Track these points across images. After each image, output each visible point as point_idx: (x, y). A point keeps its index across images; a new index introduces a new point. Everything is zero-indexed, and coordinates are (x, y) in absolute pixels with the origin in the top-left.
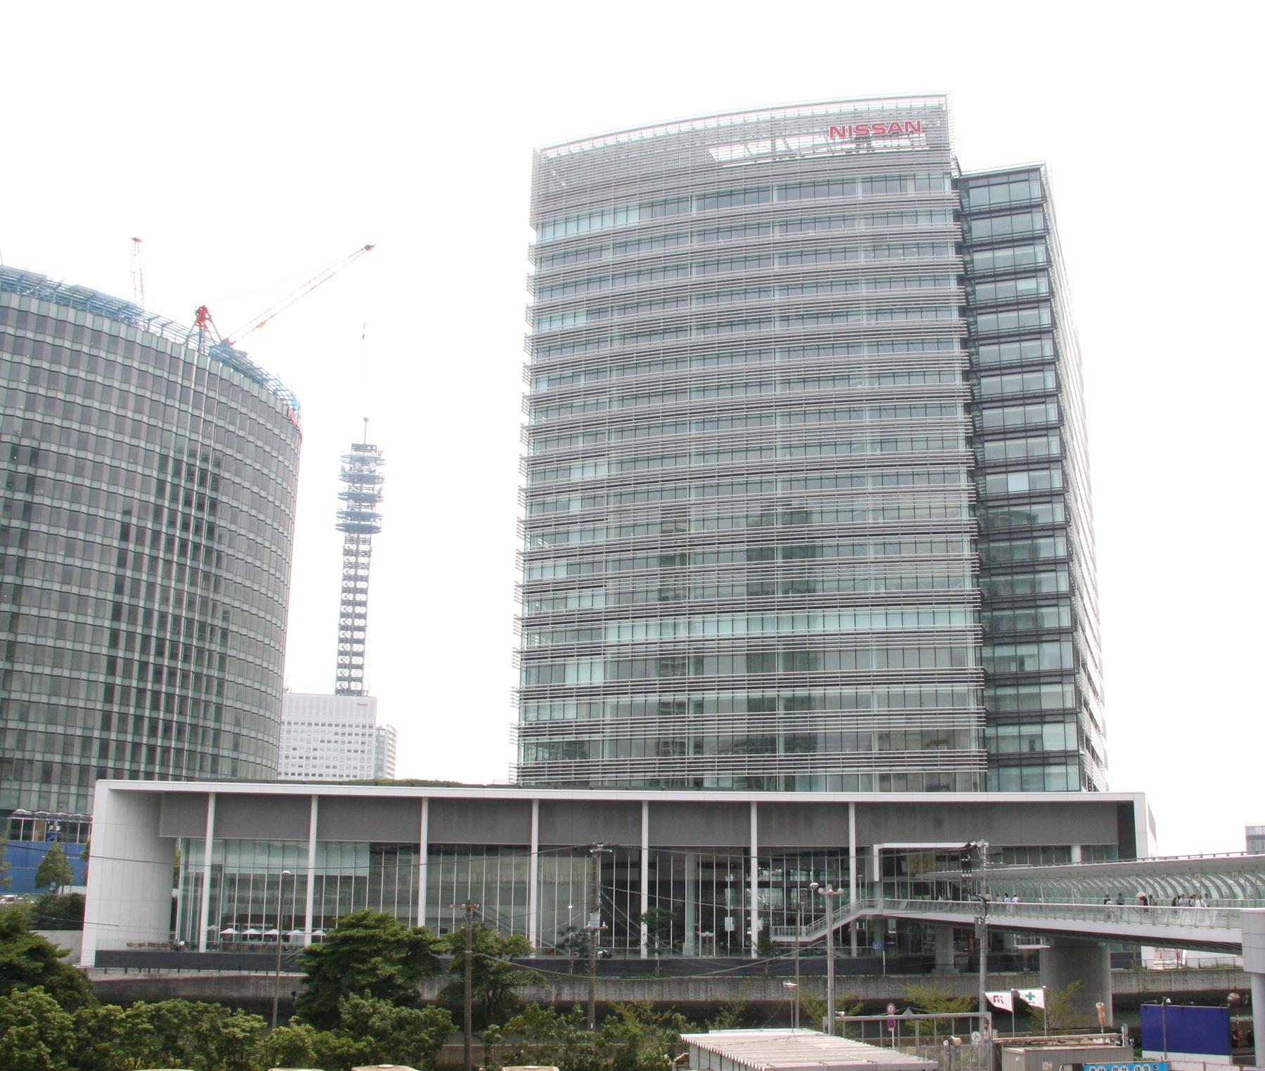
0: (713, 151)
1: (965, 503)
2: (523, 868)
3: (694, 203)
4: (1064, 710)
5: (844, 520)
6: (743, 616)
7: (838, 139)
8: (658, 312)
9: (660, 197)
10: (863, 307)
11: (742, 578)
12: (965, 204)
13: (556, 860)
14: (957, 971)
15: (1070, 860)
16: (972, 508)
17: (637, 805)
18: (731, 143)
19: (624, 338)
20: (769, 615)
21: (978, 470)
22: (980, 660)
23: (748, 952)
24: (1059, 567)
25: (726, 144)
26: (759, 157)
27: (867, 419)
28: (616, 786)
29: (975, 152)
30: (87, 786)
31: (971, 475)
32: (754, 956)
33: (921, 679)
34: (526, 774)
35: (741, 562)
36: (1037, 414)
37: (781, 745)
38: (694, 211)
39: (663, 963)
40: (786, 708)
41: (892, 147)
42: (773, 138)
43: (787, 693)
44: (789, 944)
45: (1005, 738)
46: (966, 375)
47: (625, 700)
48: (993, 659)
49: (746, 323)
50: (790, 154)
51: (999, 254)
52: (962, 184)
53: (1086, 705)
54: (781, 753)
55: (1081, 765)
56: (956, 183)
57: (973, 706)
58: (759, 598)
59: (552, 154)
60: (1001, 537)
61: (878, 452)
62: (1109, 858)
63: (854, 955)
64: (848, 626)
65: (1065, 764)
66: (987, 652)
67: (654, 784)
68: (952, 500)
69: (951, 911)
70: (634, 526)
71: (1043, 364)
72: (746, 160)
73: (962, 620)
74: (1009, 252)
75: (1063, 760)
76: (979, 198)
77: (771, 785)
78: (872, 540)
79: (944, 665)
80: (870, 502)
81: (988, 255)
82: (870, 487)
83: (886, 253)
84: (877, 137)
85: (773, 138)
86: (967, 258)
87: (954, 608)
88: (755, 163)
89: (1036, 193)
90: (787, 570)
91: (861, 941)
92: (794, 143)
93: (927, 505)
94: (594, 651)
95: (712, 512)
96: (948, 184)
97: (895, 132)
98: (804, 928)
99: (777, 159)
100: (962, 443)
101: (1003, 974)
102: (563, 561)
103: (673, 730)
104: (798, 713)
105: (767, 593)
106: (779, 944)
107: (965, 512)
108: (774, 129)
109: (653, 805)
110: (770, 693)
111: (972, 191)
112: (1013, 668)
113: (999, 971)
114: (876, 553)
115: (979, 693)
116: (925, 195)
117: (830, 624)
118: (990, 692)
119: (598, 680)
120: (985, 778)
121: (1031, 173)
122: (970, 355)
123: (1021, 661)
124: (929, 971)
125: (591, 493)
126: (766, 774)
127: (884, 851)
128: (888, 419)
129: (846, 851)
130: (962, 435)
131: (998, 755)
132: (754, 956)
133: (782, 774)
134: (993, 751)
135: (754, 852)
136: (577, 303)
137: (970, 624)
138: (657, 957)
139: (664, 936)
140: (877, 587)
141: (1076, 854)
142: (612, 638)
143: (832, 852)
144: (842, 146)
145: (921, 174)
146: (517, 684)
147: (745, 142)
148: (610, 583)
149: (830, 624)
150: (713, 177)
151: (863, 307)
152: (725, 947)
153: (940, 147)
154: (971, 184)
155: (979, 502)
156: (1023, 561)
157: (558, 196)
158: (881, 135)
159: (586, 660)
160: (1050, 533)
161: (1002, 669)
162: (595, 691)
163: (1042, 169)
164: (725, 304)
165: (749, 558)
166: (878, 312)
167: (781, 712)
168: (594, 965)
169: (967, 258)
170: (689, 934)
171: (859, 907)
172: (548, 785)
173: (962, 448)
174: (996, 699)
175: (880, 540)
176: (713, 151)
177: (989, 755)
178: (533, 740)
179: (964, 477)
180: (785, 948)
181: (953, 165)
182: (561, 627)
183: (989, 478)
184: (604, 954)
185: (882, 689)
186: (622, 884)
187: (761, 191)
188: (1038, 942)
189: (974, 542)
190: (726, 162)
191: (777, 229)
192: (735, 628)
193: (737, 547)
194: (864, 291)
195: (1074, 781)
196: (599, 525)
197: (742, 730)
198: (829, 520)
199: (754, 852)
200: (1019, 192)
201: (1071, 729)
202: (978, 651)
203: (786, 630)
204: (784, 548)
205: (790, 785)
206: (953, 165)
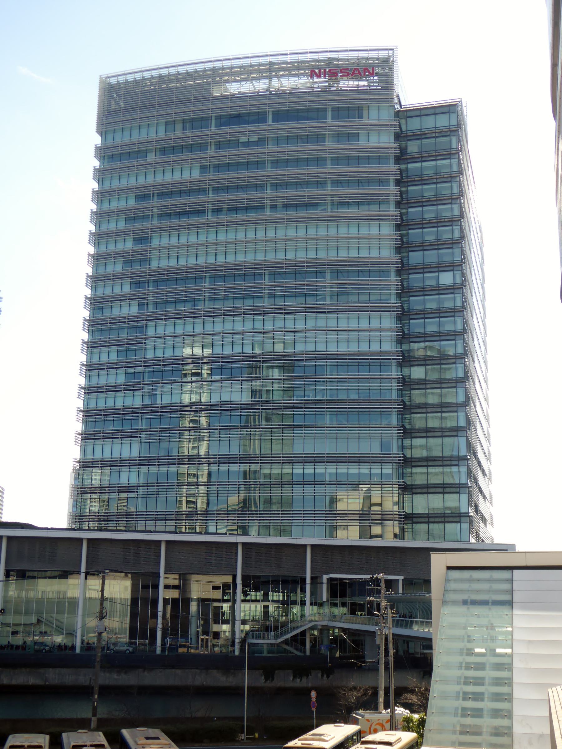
8: (186, 200)
10: (329, 200)
12: (404, 128)
29: (414, 89)
34: (78, 518)
36: (448, 325)
38: (213, 128)
46: (398, 204)
53: (476, 481)
55: (470, 494)
56: (397, 114)
59: (113, 81)
63: (308, 653)
76: (414, 125)
78: (329, 363)
79: (376, 449)
85: (270, 78)
86: (404, 189)
87: (384, 315)
88: (258, 96)
89: (457, 235)
98: (273, 633)
99: (271, 95)
102: (115, 349)
108: (271, 70)
115: (400, 471)
119: (135, 453)
121: (451, 109)
122: (402, 236)
125: (134, 324)
127: (330, 580)
128: (342, 280)
136: (128, 190)
137: (394, 325)
140: (331, 420)
146: (78, 457)
148: (146, 388)
151: (329, 200)
153: (387, 84)
156: (431, 286)
162: (136, 411)
169: (404, 189)
173: (393, 300)
175: (334, 363)
181: (396, 101)
182: (110, 418)
186: (145, 600)
187: (261, 118)
194: (329, 168)
196: (139, 347)
200: (442, 121)
202: (400, 441)
206: (396, 101)
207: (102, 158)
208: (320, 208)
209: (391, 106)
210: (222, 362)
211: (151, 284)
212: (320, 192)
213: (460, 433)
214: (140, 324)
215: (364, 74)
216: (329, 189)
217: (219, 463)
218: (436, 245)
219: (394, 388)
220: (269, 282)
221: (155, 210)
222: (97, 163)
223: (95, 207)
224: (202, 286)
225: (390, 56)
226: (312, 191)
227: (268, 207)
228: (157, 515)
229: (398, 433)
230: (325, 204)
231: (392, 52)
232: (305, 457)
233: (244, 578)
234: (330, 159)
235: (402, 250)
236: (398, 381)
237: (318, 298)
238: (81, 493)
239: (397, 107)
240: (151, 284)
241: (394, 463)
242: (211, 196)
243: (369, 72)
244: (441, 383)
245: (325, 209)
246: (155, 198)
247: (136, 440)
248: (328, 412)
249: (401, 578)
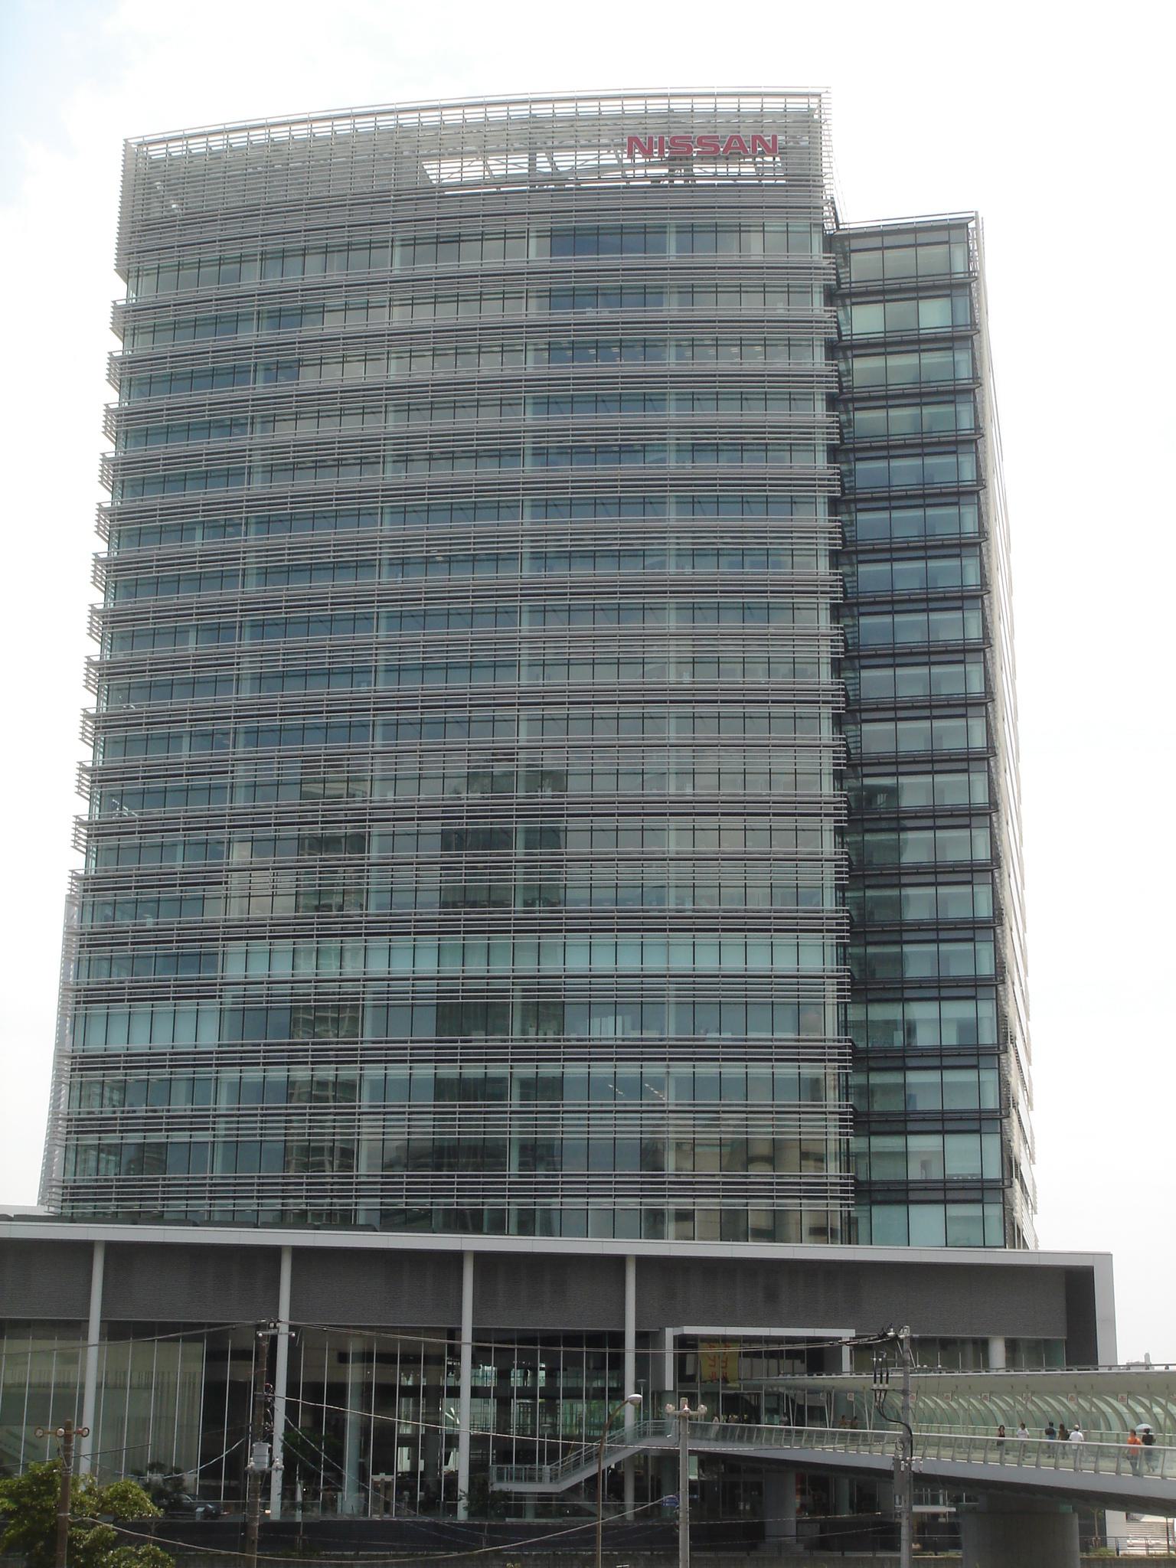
0: (431, 168)
1: (828, 767)
2: (72, 1359)
3: (397, 251)
4: (980, 1111)
5: (630, 788)
6: (431, 941)
7: (640, 159)
9: (340, 238)
11: (432, 878)
13: (130, 1346)
14: (800, 1548)
15: (986, 1365)
16: (838, 776)
17: (273, 1254)
18: (461, 155)
19: (271, 471)
20: (499, 940)
21: (851, 712)
22: (844, 1026)
23: (453, 1509)
24: (978, 877)
25: (452, 155)
26: (507, 180)
27: (672, 622)
28: (186, 1220)
29: (868, 187)
30: (812, 1238)
31: (838, 721)
32: (462, 1515)
33: (747, 1053)
34: (73, 1195)
35: (432, 850)
37: (514, 1157)
39: (309, 1527)
40: (524, 1096)
41: (727, 177)
42: (532, 152)
43: (526, 1071)
44: (520, 1496)
45: (881, 1155)
47: (254, 1075)
48: (866, 1025)
49: (477, 456)
50: (556, 176)
51: (894, 361)
52: (840, 243)
54: (513, 1170)
57: (831, 1099)
58: (469, 908)
59: (157, 152)
60: (884, 825)
61: (687, 678)
62: (1051, 1364)
64: (629, 962)
65: (981, 1201)
66: (855, 1013)
67: (301, 1220)
68: (806, 761)
69: (741, 1438)
70: (278, 784)
71: (960, 546)
72: (486, 184)
73: (815, 956)
74: (911, 360)
75: (976, 1195)
77: (498, 1226)
80: (672, 760)
81: (877, 362)
82: (672, 735)
83: (712, 351)
84: (703, 158)
85: (532, 152)
90: (530, 866)
91: (640, 1496)
92: (565, 161)
93: (791, 768)
94: (204, 992)
95: (409, 765)
96: (817, 241)
97: (734, 148)
98: (547, 1468)
100: (826, 670)
101: (880, 1555)
103: (468, 1125)
104: (543, 1104)
105: (495, 904)
106: (506, 1495)
107: (828, 782)
109: (300, 1254)
110: (497, 1070)
111: (855, 257)
112: (899, 1039)
113: (874, 1550)
114: (678, 844)
116: (779, 257)
117: (577, 958)
118: (858, 1079)
119: (209, 1039)
120: (850, 1223)
121: (954, 232)
123: (910, 1029)
124: (754, 1547)
126: (489, 1204)
128: (706, 625)
129: (618, 1339)
130: (826, 657)
131: (870, 1183)
132: (462, 1515)
133: (513, 1206)
134: (862, 1177)
135: (467, 1335)
137: (831, 965)
138: (299, 1517)
139: (310, 1477)
140: (680, 900)
141: (998, 1351)
142: (234, 970)
143: (595, 1339)
144: (645, 170)
145: (775, 224)
147: (484, 153)
149: (577, 958)
150: (427, 210)
152: (412, 1503)
153: (804, 181)
154: (855, 244)
155: (851, 765)
157: (167, 224)
158: (713, 157)
159: (144, 1008)
160: (960, 657)
161: (878, 1041)
163: (972, 225)
164: (443, 422)
165: (446, 846)
166: (696, 449)
167: (515, 1102)
168: (256, 1535)
170: (349, 1474)
171: (641, 1434)
172: (114, 1219)
174: (867, 1092)
176: (431, 168)
177: (857, 1183)
178: (91, 1140)
179: (826, 725)
180: (513, 1505)
183: (866, 727)
184: (207, 1513)
185: (683, 1069)
188: (935, 1501)
189: (839, 832)
190: (449, 186)
191: (533, 302)
192: (420, 961)
193: (428, 826)
195: (995, 1234)
197: (425, 1131)
198: (605, 786)
199: (467, 1335)
200: (930, 259)
201: (992, 1143)
203: (527, 965)
204: (528, 831)
205: (526, 1225)
206: (827, 211)
207: (126, 384)
208: (650, 457)
209: (816, 225)
210: (419, 819)
211: (247, 631)
212: (651, 418)
213: (982, 992)
214: (221, 726)
215: (754, 150)
216: (673, 413)
217: (412, 1061)
218: (922, 600)
219: (829, 1001)
220: (533, 524)
221: (257, 457)
222: (112, 397)
223: (104, 547)
224: (371, 637)
225: (813, 110)
226: (632, 417)
227: (528, 452)
228: (263, 1184)
229: (839, 990)
230: (662, 553)
231: (816, 100)
232: (617, 1183)
233: (477, 1334)
234: (673, 500)
235: (843, 559)
236: (836, 866)
237: (648, 561)
238: (76, 1132)
239: (829, 226)
240: (247, 631)
241: (828, 931)
242: (387, 528)
243: (764, 144)
244: (937, 930)
245: (663, 460)
246: (252, 528)
247: (212, 1005)
248: (674, 822)
249: (847, 1334)
